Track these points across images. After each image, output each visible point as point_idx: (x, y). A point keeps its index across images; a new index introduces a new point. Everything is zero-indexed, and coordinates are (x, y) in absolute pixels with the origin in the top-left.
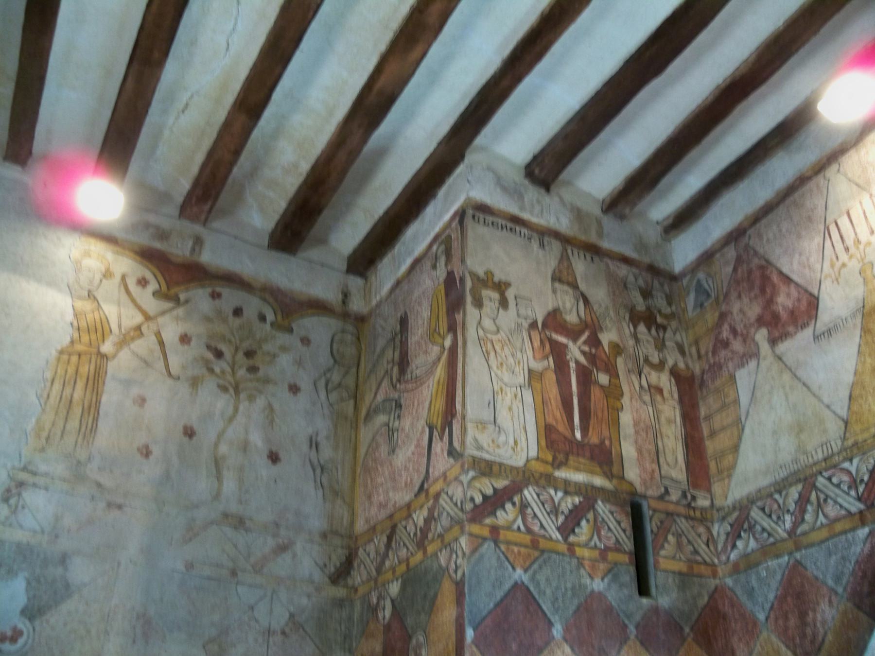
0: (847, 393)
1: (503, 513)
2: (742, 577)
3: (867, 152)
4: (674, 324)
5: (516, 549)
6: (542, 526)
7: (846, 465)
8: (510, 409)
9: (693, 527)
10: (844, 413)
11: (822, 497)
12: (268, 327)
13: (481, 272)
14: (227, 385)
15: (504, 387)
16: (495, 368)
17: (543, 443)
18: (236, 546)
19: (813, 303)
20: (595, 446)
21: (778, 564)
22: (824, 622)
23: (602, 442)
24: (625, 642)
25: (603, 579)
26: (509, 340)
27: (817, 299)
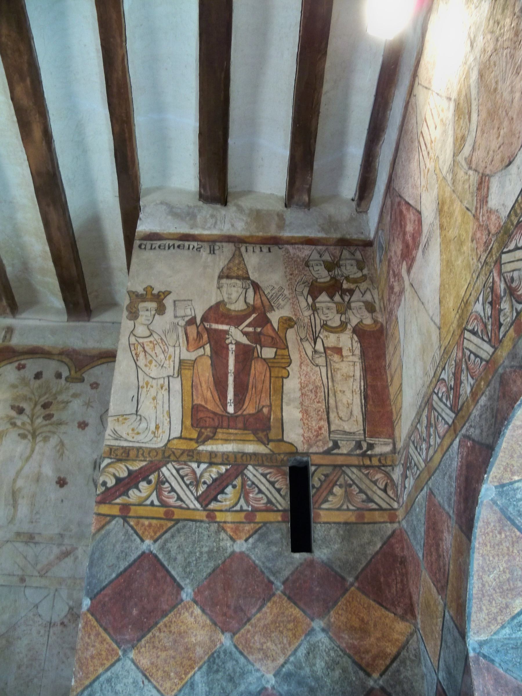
1: (135, 491)
5: (146, 522)
6: (179, 498)
9: (367, 475)
12: (63, 381)
14: (26, 433)
17: (188, 423)
18: (25, 558)
23: (260, 411)
24: (269, 600)
25: (246, 540)
26: (161, 339)
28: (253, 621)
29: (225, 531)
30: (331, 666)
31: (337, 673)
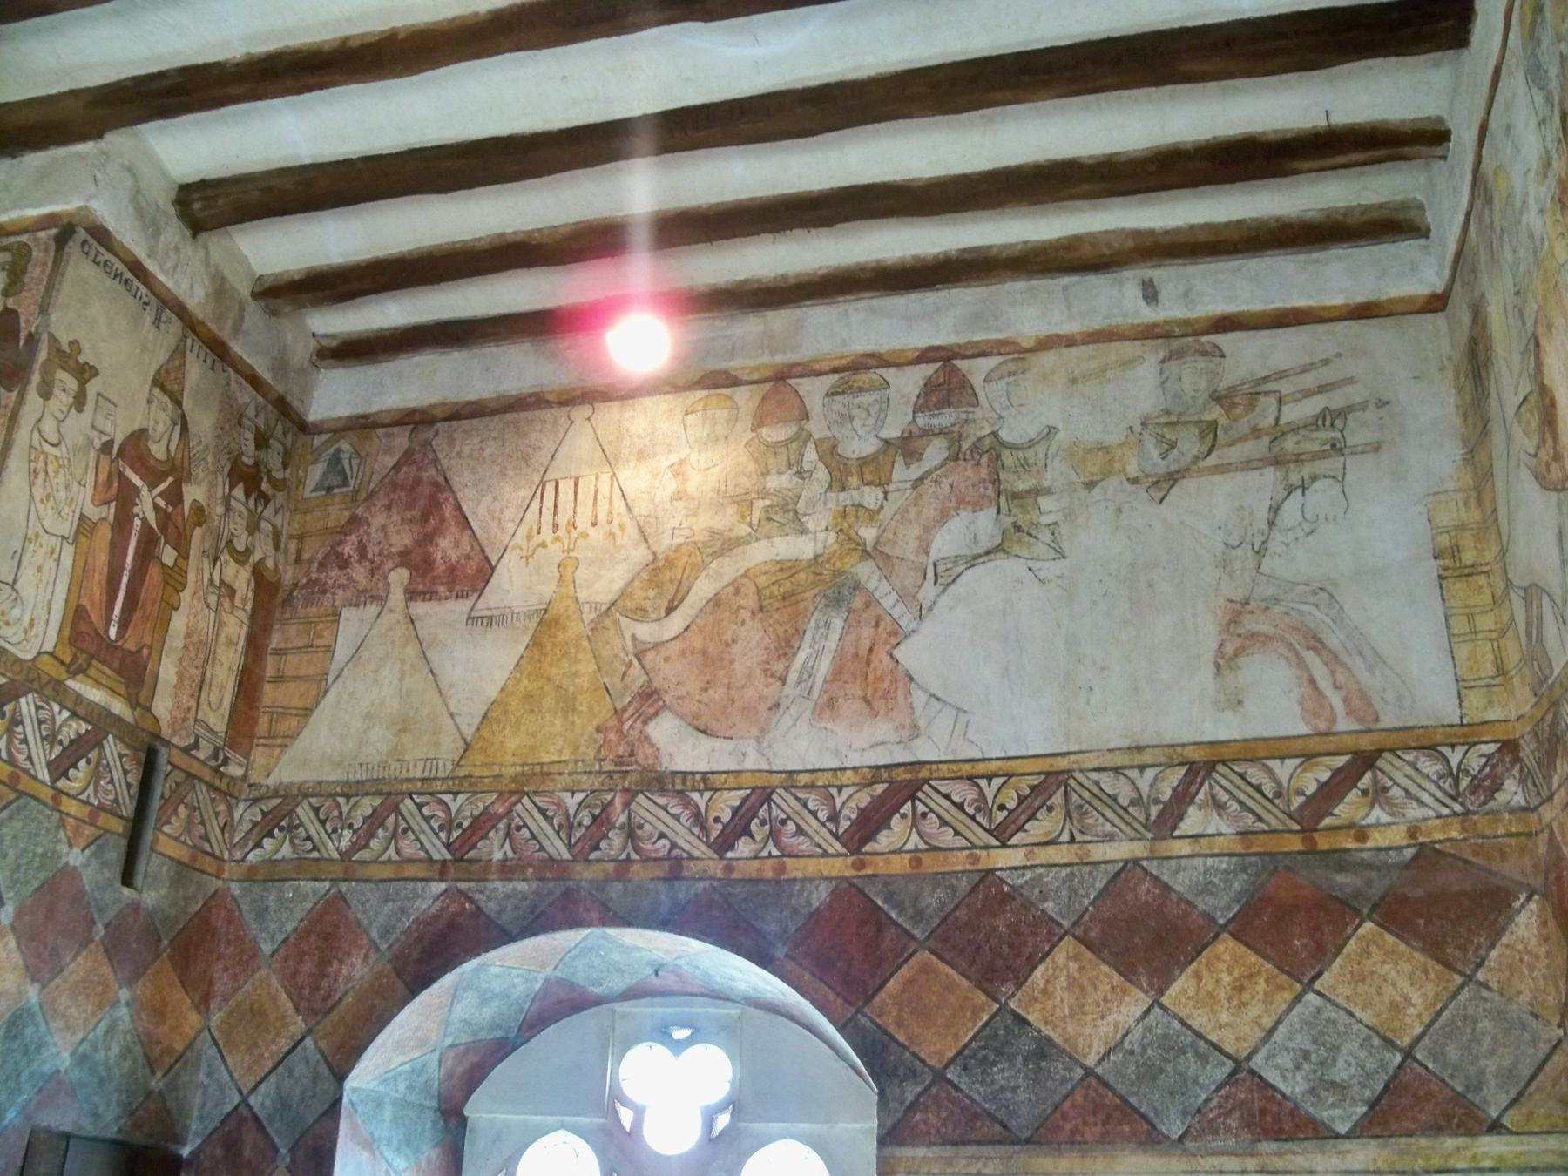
0: (484, 708)
2: (257, 889)
3: (633, 418)
4: (280, 497)
6: (29, 758)
7: (447, 798)
8: (39, 569)
9: (213, 800)
10: (469, 732)
11: (403, 825)
13: (64, 340)
15: (41, 532)
16: (37, 500)
17: (66, 633)
19: (485, 572)
20: (130, 652)
21: (312, 890)
22: (349, 979)
23: (139, 651)
25: (83, 850)
27: (493, 569)
28: (66, 973)
29: (65, 830)
30: (126, 1052)
31: (127, 1065)
